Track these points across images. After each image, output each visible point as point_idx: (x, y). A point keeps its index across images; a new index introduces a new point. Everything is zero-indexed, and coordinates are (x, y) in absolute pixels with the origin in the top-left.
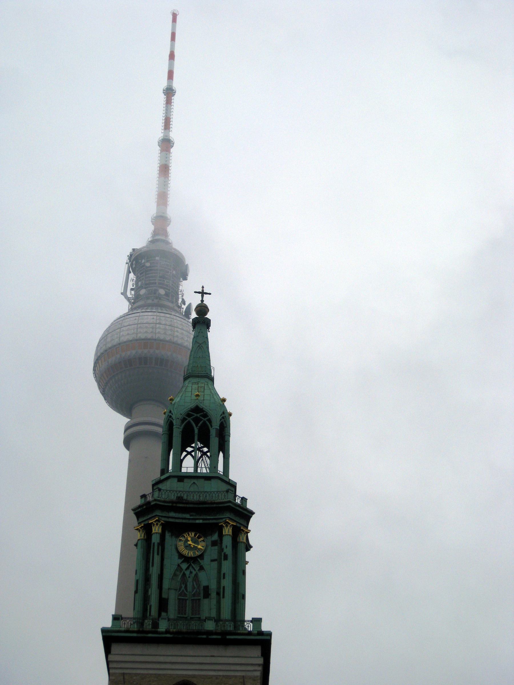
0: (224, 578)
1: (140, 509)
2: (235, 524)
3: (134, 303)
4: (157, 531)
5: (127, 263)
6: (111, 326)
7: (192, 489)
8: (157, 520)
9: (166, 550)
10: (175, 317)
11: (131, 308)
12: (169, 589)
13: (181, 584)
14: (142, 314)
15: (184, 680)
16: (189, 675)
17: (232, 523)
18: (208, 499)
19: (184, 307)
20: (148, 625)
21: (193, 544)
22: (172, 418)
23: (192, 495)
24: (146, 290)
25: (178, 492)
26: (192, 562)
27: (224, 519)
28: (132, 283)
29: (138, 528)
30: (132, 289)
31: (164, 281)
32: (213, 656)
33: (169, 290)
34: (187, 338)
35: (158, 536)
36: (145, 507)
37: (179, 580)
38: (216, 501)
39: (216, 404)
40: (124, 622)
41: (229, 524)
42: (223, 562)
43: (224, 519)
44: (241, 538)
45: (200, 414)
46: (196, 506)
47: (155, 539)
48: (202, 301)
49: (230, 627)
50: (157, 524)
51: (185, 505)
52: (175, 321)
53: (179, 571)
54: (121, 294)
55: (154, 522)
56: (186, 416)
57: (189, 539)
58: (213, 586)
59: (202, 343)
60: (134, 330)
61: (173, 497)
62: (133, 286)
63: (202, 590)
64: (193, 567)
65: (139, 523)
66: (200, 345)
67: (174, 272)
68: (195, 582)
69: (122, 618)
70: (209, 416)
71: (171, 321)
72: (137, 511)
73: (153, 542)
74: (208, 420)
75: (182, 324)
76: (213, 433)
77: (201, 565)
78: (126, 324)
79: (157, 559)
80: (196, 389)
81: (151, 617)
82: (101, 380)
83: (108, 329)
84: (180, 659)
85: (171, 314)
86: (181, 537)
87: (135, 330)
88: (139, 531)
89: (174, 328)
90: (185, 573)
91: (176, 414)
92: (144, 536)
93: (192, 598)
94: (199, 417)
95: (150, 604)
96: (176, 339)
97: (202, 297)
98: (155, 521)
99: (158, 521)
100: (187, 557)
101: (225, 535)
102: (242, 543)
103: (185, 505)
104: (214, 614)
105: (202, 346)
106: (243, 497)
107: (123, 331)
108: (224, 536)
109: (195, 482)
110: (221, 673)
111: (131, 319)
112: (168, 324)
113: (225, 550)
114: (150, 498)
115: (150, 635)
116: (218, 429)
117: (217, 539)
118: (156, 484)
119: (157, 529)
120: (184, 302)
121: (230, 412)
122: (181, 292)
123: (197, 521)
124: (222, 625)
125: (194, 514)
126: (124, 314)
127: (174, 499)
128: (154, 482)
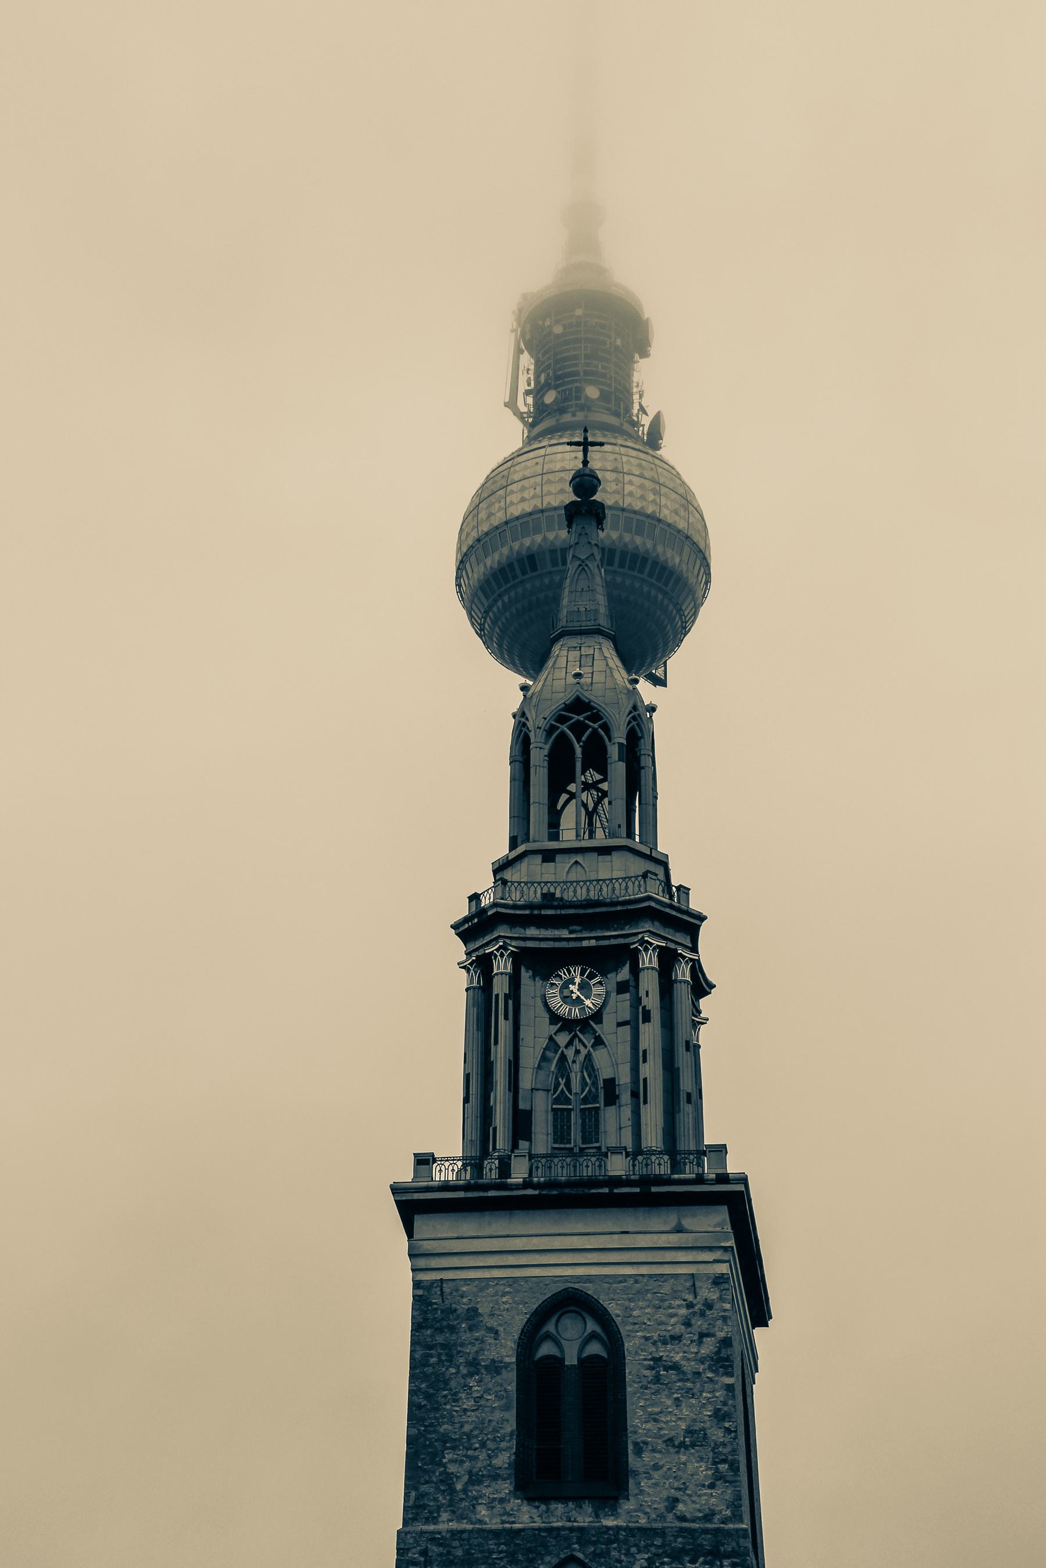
0: (645, 1061)
1: (466, 926)
2: (664, 945)
3: (532, 425)
4: (502, 970)
5: (513, 331)
6: (486, 483)
7: (573, 877)
8: (500, 947)
9: (523, 1009)
10: (623, 450)
11: (527, 437)
12: (532, 1089)
13: (557, 1078)
14: (550, 450)
15: (567, 1289)
16: (578, 1277)
17: (656, 943)
18: (606, 893)
19: (646, 421)
20: (491, 1171)
21: (578, 993)
22: (528, 729)
23: (572, 889)
24: (558, 392)
25: (543, 884)
26: (578, 1029)
27: (640, 936)
28: (526, 379)
29: (466, 965)
30: (527, 393)
31: (597, 366)
32: (627, 1233)
33: (609, 386)
34: (655, 494)
35: (506, 980)
36: (476, 920)
37: (552, 1070)
38: (620, 899)
39: (618, 692)
40: (438, 1168)
41: (651, 944)
42: (641, 1026)
43: (640, 936)
44: (680, 974)
45: (583, 715)
46: (582, 911)
47: (500, 987)
48: (585, 463)
49: (662, 1167)
50: (502, 955)
51: (559, 912)
52: (625, 459)
53: (553, 1050)
54: (506, 406)
55: (495, 952)
56: (556, 722)
57: (578, 980)
58: (624, 1078)
59: (587, 559)
60: (535, 489)
61: (534, 895)
62: (529, 384)
63: (601, 1088)
64: (580, 1041)
65: (468, 954)
66: (583, 562)
67: (619, 342)
68: (586, 1071)
69: (435, 1160)
70: (604, 717)
71: (616, 459)
72: (461, 929)
73: (496, 993)
74: (601, 726)
75: (640, 466)
76: (613, 752)
77: (597, 1034)
78: (516, 477)
79: (504, 1027)
80: (575, 661)
81: (497, 1154)
82: (476, 600)
83: (480, 492)
84: (557, 1243)
85: (615, 444)
86: (554, 977)
87: (538, 489)
88: (468, 971)
89: (622, 474)
90: (566, 1054)
91: (536, 719)
92: (479, 982)
93: (582, 1107)
94: (583, 721)
95: (493, 1123)
96: (628, 500)
97: (585, 452)
98: (497, 950)
99: (504, 947)
100: (568, 1019)
101: (644, 969)
102: (682, 983)
103: (559, 912)
104: (628, 1141)
105: (586, 565)
106: (680, 885)
107: (512, 492)
108: (642, 971)
109: (578, 860)
110: (644, 1270)
111: (528, 464)
112: (609, 468)
113: (645, 1001)
114: (485, 902)
115: (492, 1193)
116: (623, 744)
117: (628, 978)
118: (500, 868)
119: (502, 966)
120: (642, 409)
121: (653, 703)
122: (637, 386)
123: (585, 943)
124: (642, 1163)
125: (578, 928)
126: (513, 453)
127: (535, 900)
128: (497, 866)
